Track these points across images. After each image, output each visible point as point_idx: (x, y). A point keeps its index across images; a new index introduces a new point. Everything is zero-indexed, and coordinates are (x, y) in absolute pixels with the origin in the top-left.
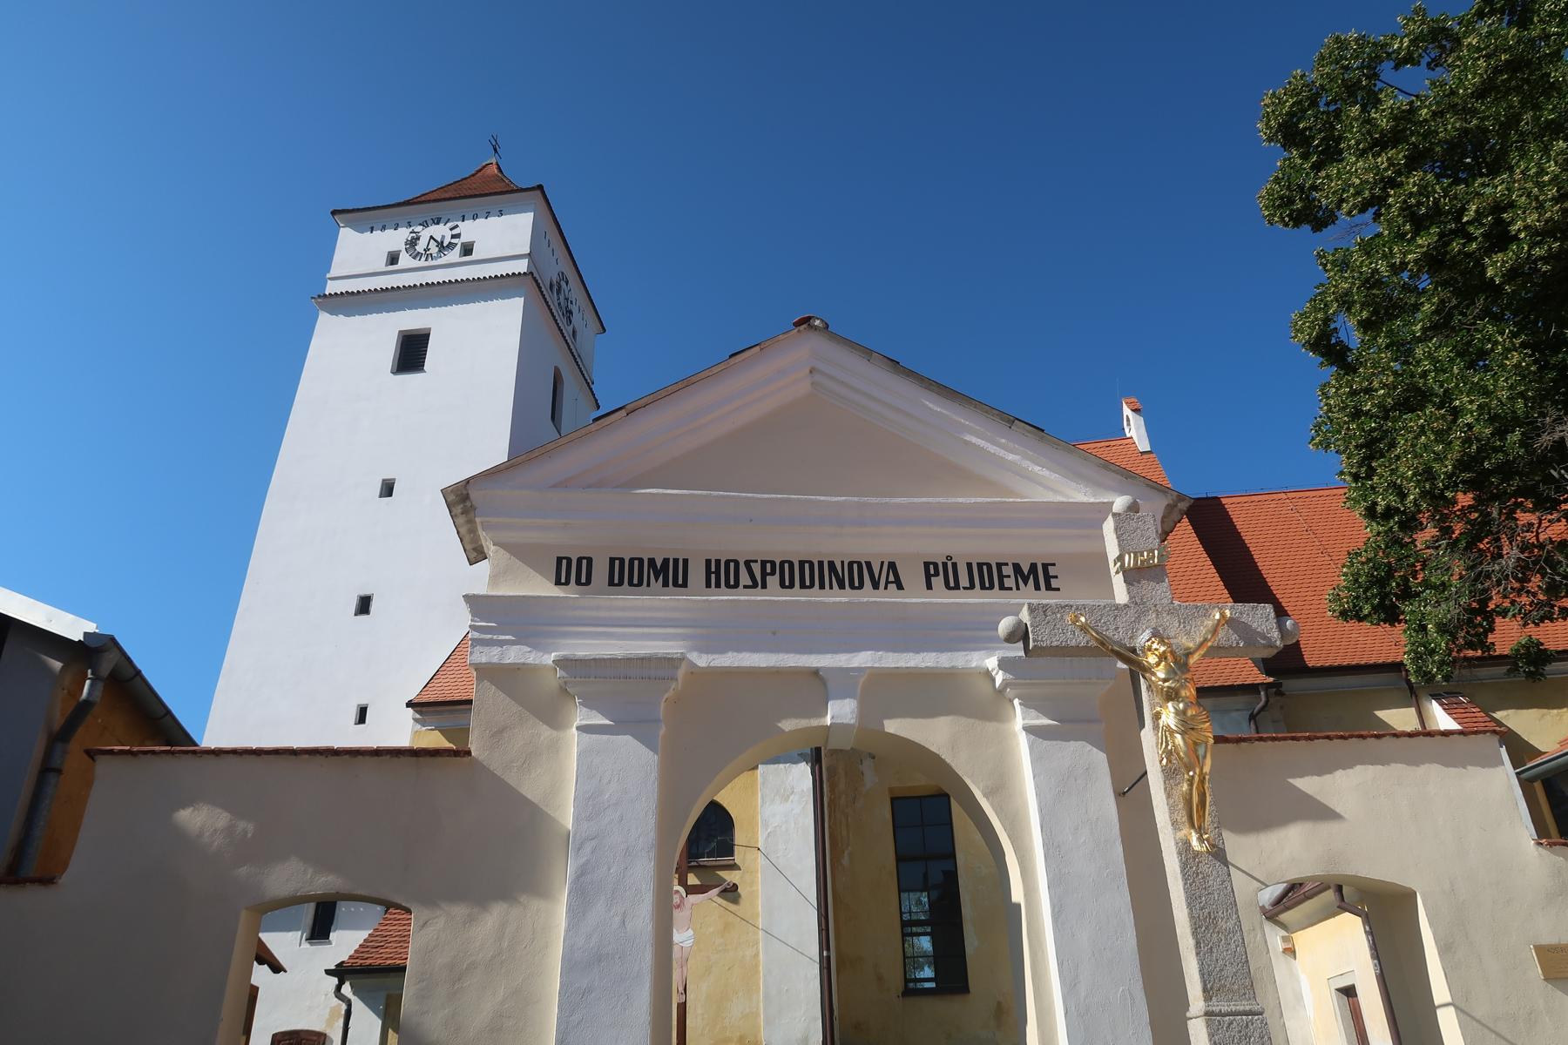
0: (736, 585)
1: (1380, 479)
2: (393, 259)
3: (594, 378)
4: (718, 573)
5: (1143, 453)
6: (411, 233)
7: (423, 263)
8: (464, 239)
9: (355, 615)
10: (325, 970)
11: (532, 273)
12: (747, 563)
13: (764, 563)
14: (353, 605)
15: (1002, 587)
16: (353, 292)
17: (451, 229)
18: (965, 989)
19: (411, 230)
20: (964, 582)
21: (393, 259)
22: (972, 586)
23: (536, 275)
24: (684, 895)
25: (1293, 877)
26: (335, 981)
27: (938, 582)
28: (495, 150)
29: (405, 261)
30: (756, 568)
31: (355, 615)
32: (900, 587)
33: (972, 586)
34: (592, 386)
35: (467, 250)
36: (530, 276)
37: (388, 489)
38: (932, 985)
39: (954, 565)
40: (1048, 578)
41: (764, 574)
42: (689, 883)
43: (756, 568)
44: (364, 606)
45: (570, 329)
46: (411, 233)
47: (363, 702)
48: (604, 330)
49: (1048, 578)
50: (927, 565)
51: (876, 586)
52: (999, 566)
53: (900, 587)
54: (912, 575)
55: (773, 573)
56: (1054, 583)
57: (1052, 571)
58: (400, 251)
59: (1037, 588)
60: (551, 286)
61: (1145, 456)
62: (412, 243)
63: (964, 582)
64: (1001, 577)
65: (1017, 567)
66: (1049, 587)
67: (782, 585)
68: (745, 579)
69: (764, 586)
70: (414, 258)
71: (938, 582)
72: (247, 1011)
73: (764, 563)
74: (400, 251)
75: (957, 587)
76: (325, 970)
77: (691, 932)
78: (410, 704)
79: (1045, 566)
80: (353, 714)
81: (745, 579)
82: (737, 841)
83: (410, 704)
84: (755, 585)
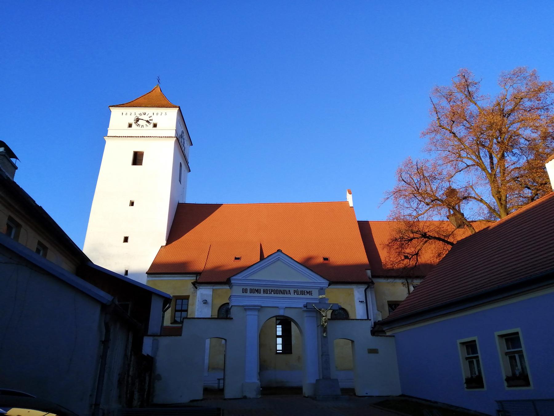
0: (267, 293)
1: (495, 130)
2: (130, 126)
3: (189, 161)
4: (265, 291)
5: (350, 207)
12: (269, 290)
13: (271, 290)
14: (123, 239)
15: (305, 295)
17: (149, 117)
18: (291, 353)
19: (136, 116)
20: (299, 294)
22: (300, 294)
27: (296, 293)
28: (159, 81)
30: (270, 291)
32: (290, 294)
33: (300, 294)
34: (188, 164)
35: (155, 126)
37: (132, 204)
38: (281, 352)
39: (298, 291)
40: (311, 293)
41: (271, 292)
43: (270, 291)
48: (192, 145)
49: (311, 293)
50: (294, 291)
51: (287, 294)
52: (304, 291)
53: (290, 294)
54: (292, 292)
55: (273, 291)
56: (312, 294)
57: (312, 292)
59: (309, 295)
60: (180, 136)
61: (351, 208)
62: (137, 120)
63: (299, 294)
64: (305, 293)
65: (307, 291)
66: (311, 295)
67: (274, 294)
68: (269, 292)
69: (271, 294)
70: (137, 126)
71: (296, 293)
73: (271, 290)
75: (298, 294)
79: (311, 291)
81: (269, 292)
84: (270, 293)
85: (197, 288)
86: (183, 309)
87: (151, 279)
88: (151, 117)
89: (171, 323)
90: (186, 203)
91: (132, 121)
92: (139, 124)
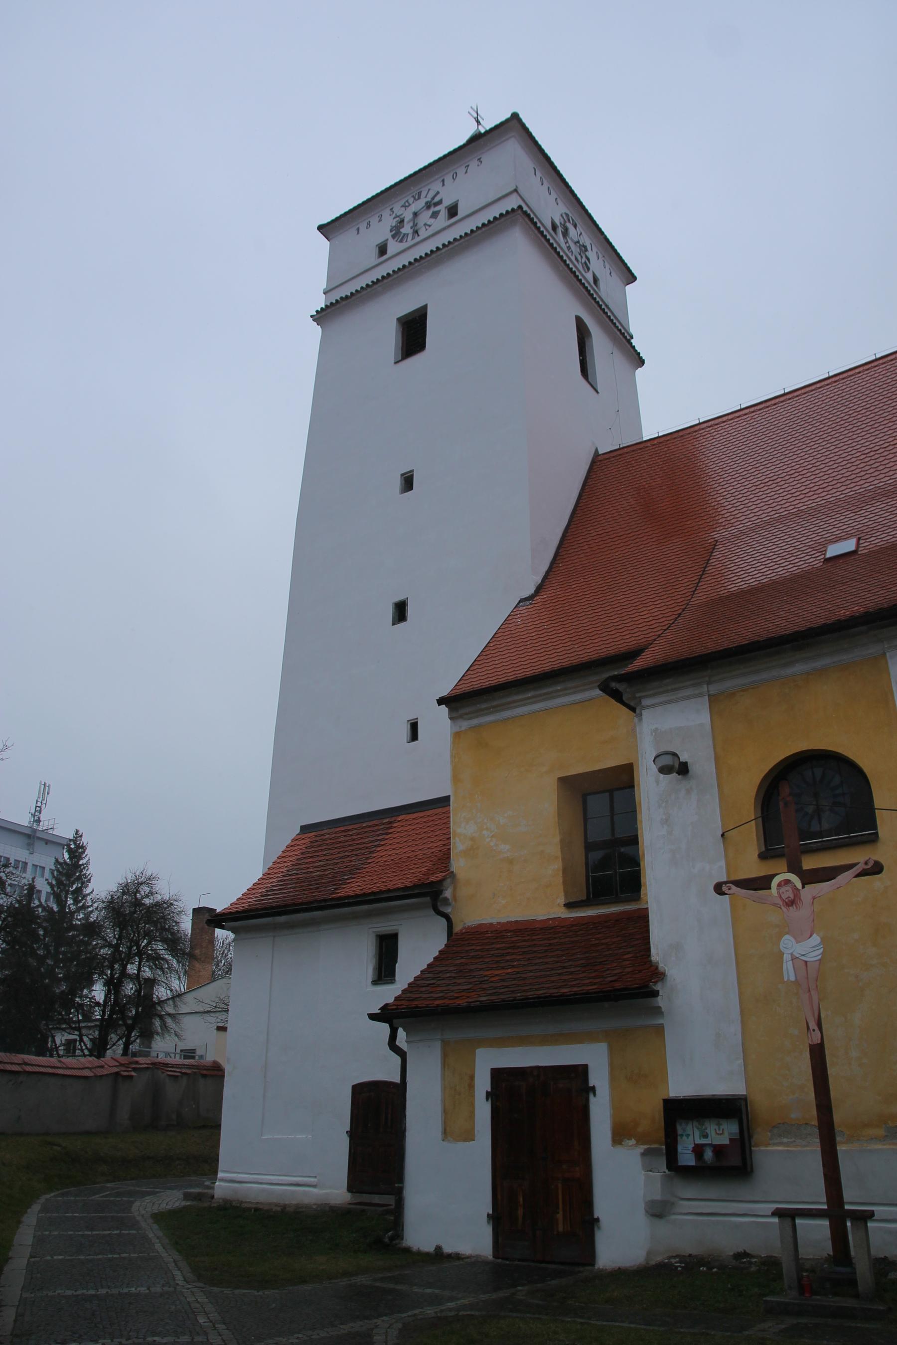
2: (382, 250)
3: (632, 330)
6: (394, 218)
7: (410, 242)
8: (447, 202)
9: (393, 624)
10: (321, 228)
11: (520, 207)
14: (389, 612)
16: (347, 296)
19: (394, 215)
21: (382, 250)
23: (525, 208)
24: (799, 884)
25: (440, 1122)
26: (385, 1028)
29: (393, 247)
31: (393, 624)
35: (453, 211)
36: (520, 212)
42: (805, 868)
44: (400, 612)
45: (589, 276)
46: (394, 218)
47: (412, 717)
48: (634, 278)
58: (388, 240)
60: (554, 227)
62: (396, 232)
72: (491, 1046)
74: (388, 240)
76: (321, 228)
77: (816, 939)
78: (441, 701)
80: (405, 731)
82: (877, 803)
83: (441, 701)
85: (633, 710)
86: (617, 836)
87: (465, 724)
88: (438, 193)
89: (569, 906)
90: (645, 439)
91: (389, 235)
92: (404, 234)
